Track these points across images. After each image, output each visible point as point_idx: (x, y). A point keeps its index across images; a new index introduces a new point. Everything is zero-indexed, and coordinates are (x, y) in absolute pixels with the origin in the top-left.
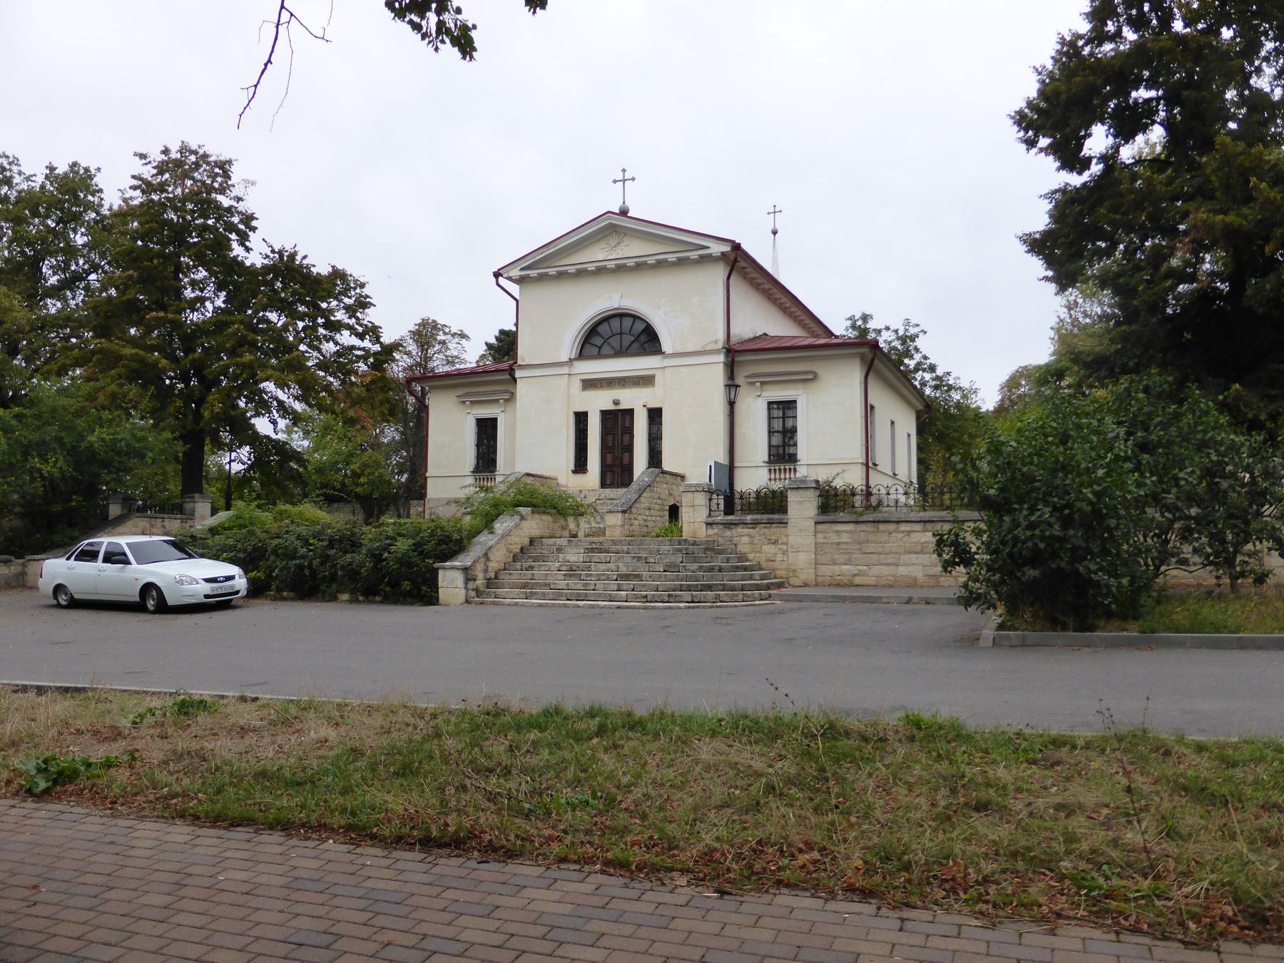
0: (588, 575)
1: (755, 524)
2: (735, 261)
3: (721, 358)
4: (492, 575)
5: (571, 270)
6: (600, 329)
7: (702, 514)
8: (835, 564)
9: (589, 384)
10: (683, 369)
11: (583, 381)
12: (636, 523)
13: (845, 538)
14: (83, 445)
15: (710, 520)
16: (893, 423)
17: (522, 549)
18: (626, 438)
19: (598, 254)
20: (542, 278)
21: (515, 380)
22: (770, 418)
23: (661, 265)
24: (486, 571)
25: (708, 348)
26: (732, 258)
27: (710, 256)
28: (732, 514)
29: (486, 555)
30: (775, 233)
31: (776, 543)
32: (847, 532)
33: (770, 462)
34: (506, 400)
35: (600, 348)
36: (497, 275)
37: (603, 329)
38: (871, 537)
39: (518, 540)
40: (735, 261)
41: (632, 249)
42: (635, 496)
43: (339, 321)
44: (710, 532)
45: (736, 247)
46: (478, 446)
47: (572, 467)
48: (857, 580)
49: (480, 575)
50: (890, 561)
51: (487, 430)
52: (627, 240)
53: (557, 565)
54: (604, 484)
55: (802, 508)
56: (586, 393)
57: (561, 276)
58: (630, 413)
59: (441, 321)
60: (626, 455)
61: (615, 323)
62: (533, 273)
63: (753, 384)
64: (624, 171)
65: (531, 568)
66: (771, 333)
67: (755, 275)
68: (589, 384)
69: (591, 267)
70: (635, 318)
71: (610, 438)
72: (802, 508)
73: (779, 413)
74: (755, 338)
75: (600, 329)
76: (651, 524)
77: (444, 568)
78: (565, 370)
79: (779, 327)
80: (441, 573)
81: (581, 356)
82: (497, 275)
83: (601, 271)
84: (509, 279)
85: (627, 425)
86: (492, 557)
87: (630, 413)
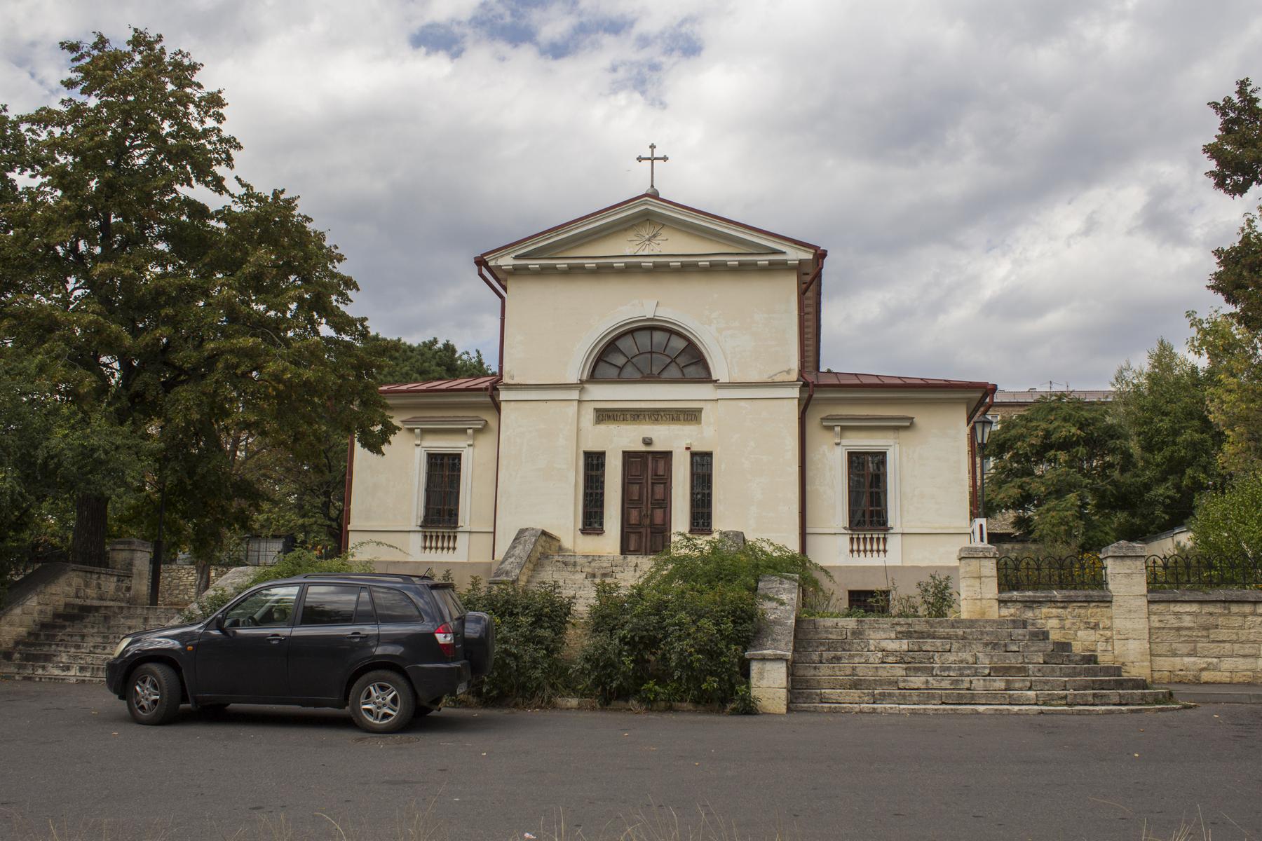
1: (1066, 602)
3: (795, 393)
5: (590, 264)
6: (621, 344)
8: (1175, 655)
9: (605, 415)
10: (742, 403)
11: (597, 410)
13: (1187, 621)
14: (41, 454)
15: (1006, 596)
18: (659, 489)
19: (624, 247)
20: (546, 272)
21: (497, 407)
23: (716, 269)
25: (778, 379)
27: (784, 263)
31: (1095, 627)
32: (1189, 613)
34: (477, 431)
35: (621, 369)
37: (626, 344)
38: (1221, 621)
41: (673, 245)
44: (1007, 612)
47: (580, 526)
48: (1206, 676)
50: (1247, 652)
51: (443, 474)
52: (665, 234)
54: (625, 550)
57: (575, 272)
58: (667, 456)
60: (659, 513)
61: (659, 337)
62: (534, 264)
63: (831, 428)
64: (653, 147)
68: (605, 415)
69: (619, 263)
70: (671, 332)
71: (636, 488)
75: (621, 344)
77: (764, 659)
78: (575, 395)
82: (820, 255)
83: (632, 270)
87: (667, 456)
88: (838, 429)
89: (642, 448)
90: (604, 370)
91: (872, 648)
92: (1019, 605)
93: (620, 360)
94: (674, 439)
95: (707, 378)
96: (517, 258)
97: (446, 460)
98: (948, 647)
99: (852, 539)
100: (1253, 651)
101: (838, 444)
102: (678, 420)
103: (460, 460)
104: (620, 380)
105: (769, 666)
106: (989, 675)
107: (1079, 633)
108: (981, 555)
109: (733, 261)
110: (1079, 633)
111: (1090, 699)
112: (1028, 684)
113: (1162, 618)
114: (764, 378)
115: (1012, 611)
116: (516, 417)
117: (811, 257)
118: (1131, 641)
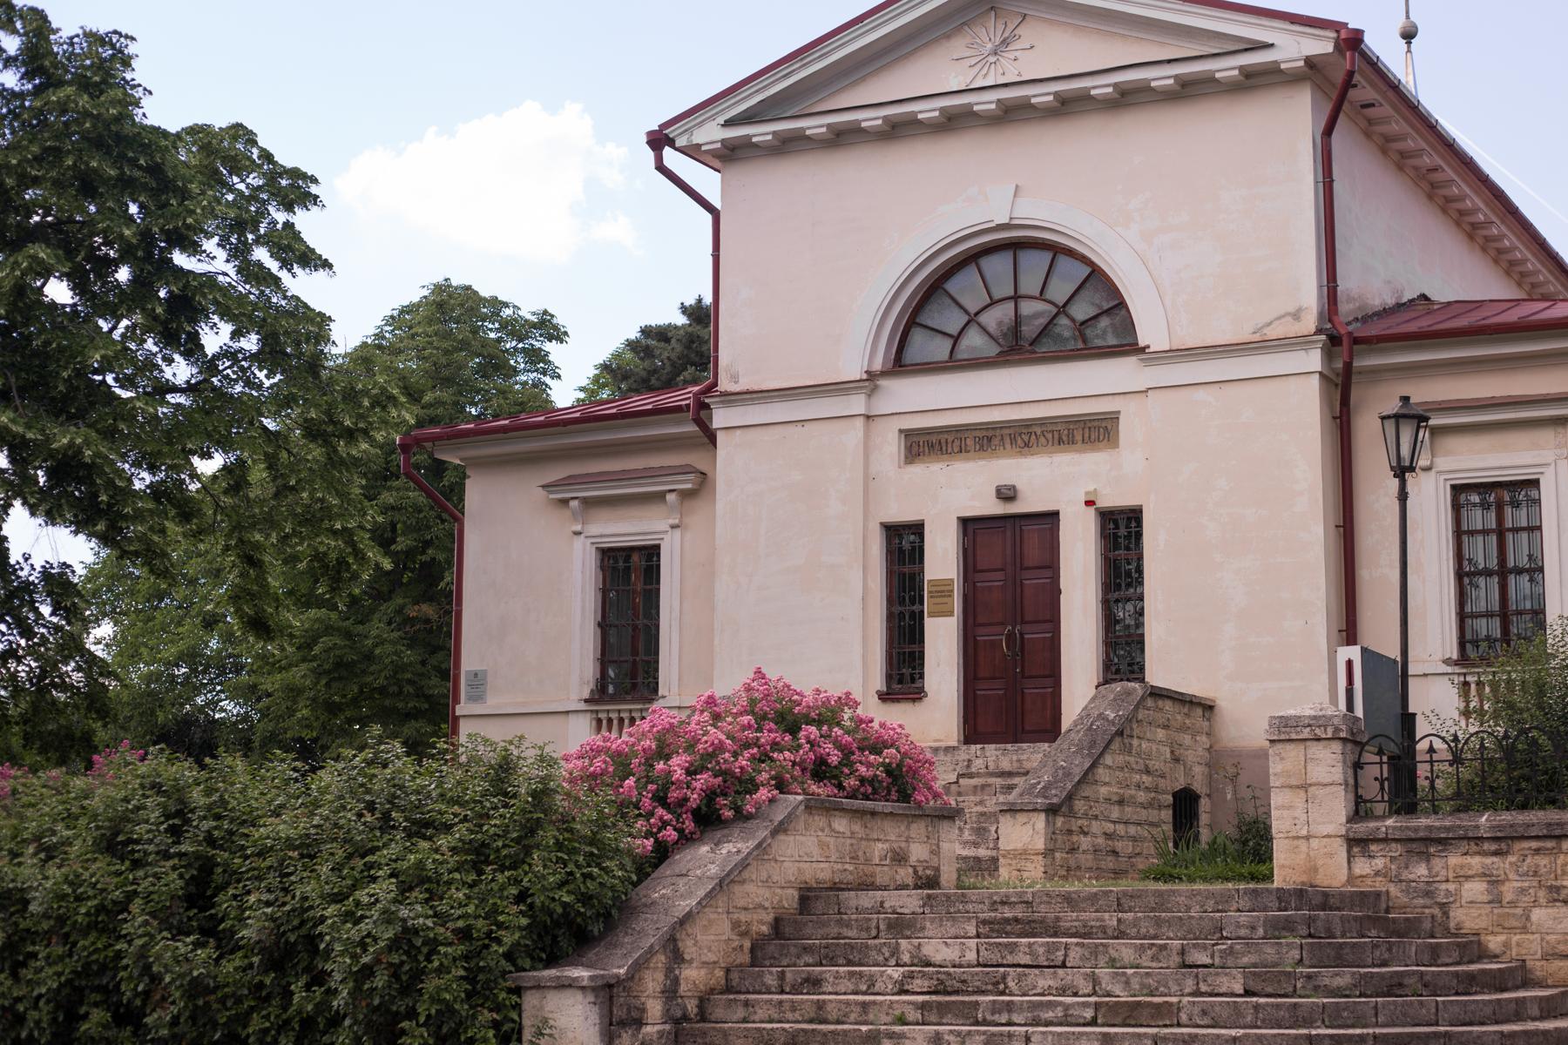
0: (996, 1008)
1: (1503, 841)
2: (1348, 84)
3: (1313, 360)
4: (692, 1007)
5: (871, 119)
7: (1333, 812)
9: (924, 444)
10: (1201, 394)
11: (907, 434)
12: (1085, 842)
15: (1363, 828)
17: (777, 923)
19: (945, 73)
20: (787, 145)
21: (711, 437)
22: (1460, 534)
23: (1129, 98)
24: (670, 992)
25: (1272, 333)
26: (1339, 77)
28: (1410, 809)
29: (672, 939)
33: (1463, 660)
34: (686, 495)
35: (956, 339)
36: (658, 141)
39: (767, 893)
40: (1348, 84)
42: (1080, 765)
43: (209, 280)
44: (1362, 867)
45: (1352, 41)
46: (604, 626)
49: (655, 1008)
51: (630, 581)
52: (1028, 34)
53: (896, 973)
54: (974, 731)
56: (918, 470)
57: (843, 138)
62: (761, 132)
65: (814, 983)
66: (1442, 292)
67: (1397, 126)
68: (924, 444)
69: (927, 111)
70: (1058, 250)
73: (1478, 519)
74: (1399, 307)
76: (1124, 847)
78: (857, 404)
79: (1456, 277)
81: (900, 365)
82: (658, 141)
84: (693, 152)
86: (689, 948)
90: (925, 347)
91: (906, 958)
92: (1396, 850)
93: (952, 321)
94: (1059, 484)
95: (1128, 346)
96: (728, 123)
97: (635, 557)
101: (578, 533)
102: (1072, 441)
103: (921, 535)
104: (954, 364)
107: (1537, 915)
108: (1306, 733)
109: (1162, 78)
110: (1537, 915)
114: (1245, 336)
115: (1379, 863)
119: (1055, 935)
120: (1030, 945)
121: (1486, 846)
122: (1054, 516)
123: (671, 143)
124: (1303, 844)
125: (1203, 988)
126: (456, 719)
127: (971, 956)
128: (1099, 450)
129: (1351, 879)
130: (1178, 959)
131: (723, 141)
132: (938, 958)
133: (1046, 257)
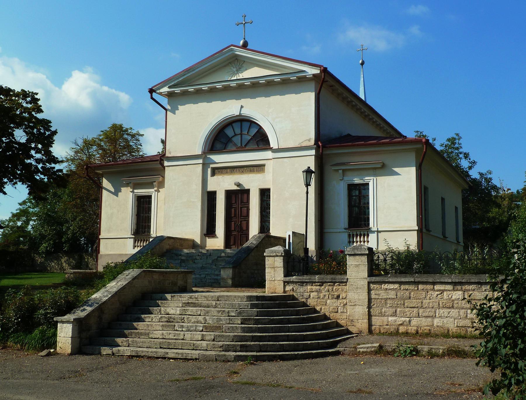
3: (313, 152)
13: (392, 295)
16: (443, 199)
20: (185, 93)
21: (164, 167)
25: (304, 145)
27: (305, 77)
30: (362, 64)
36: (151, 91)
45: (325, 70)
51: (143, 206)
55: (357, 269)
59: (125, 126)
62: (177, 90)
72: (357, 269)
77: (63, 322)
78: (201, 161)
80: (59, 325)
82: (151, 91)
84: (160, 94)
85: (245, 201)
88: (341, 171)
89: (236, 188)
90: (218, 146)
94: (253, 183)
98: (199, 313)
99: (349, 235)
100: (431, 314)
105: (65, 325)
106: (202, 331)
110: (328, 302)
111: (238, 348)
112: (213, 337)
113: (377, 292)
114: (296, 145)
116: (172, 173)
117: (319, 72)
118: (357, 307)
119: (201, 307)
120: (192, 310)
121: (317, 284)
122: (248, 190)
123: (155, 92)
124: (273, 282)
125: (231, 322)
126: (99, 239)
127: (178, 312)
128: (260, 173)
129: (285, 292)
130: (227, 315)
131: (167, 92)
132: (170, 313)
133: (249, 124)
